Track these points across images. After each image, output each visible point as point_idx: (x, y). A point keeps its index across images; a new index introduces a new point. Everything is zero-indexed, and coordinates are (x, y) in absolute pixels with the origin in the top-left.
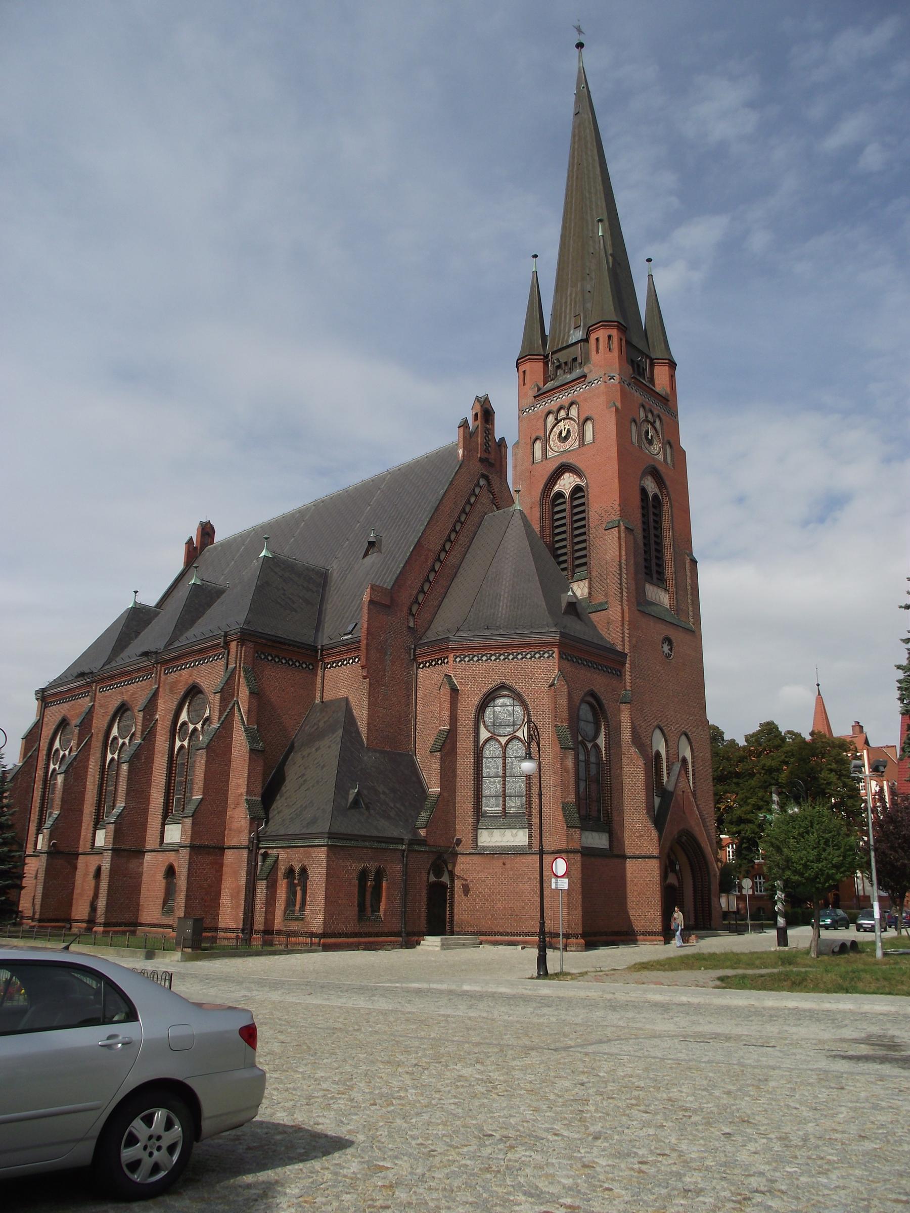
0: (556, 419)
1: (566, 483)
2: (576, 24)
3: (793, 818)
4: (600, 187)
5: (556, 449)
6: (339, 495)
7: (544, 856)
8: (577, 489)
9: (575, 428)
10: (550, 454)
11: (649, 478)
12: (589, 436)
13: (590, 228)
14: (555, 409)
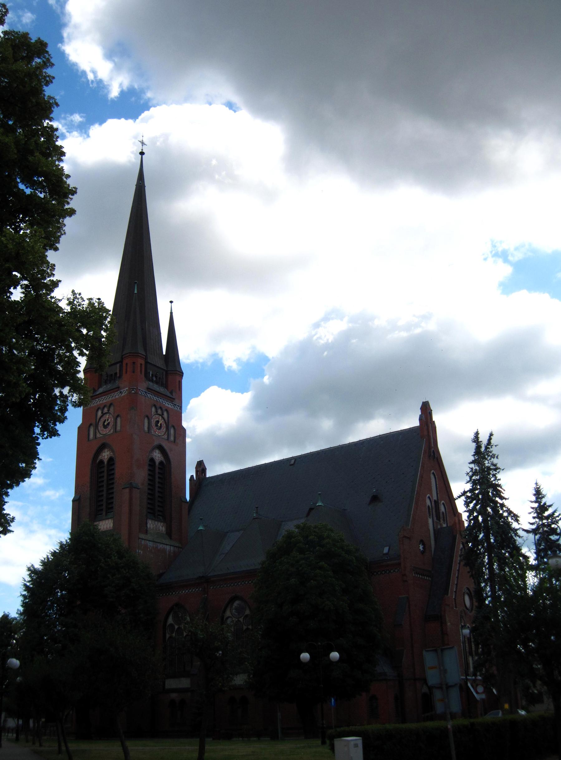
0: (102, 413)
1: (106, 455)
2: (141, 140)
3: (546, 531)
8: (111, 460)
9: (111, 420)
10: (98, 435)
11: (157, 451)
14: (102, 407)
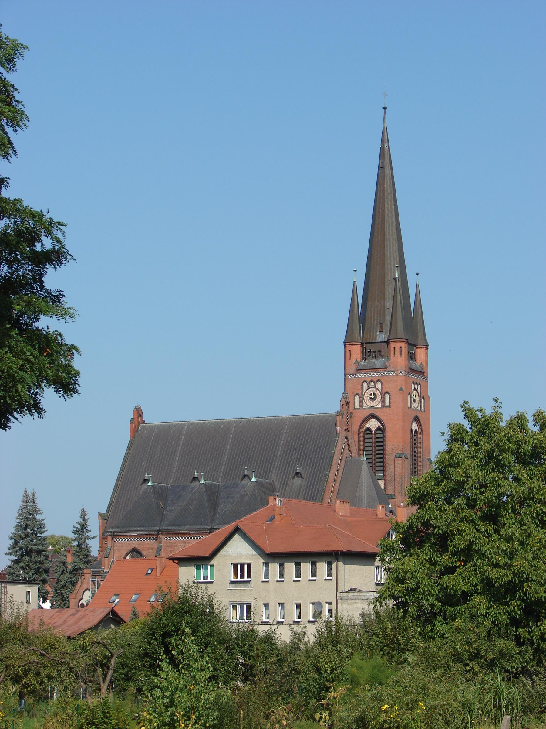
0: (369, 387)
1: (373, 424)
4: (395, 230)
5: (368, 403)
6: (270, 420)
7: (237, 536)
12: (387, 403)
13: (389, 261)
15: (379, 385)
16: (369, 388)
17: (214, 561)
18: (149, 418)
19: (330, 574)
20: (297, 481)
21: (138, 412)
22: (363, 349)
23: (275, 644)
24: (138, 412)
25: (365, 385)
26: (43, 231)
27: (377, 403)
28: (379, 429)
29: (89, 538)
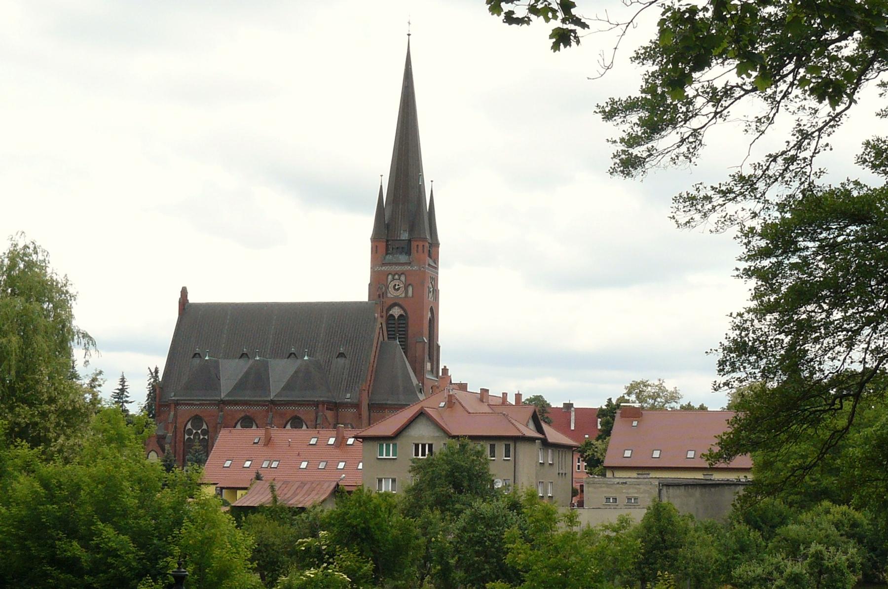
15: (403, 278)
16: (394, 279)
17: (398, 442)
18: (192, 299)
19: (507, 455)
20: (341, 361)
21: (184, 292)
22: (387, 245)
23: (370, 499)
24: (184, 292)
25: (390, 277)
26: (774, 260)
27: (401, 294)
28: (401, 315)
29: (127, 402)
